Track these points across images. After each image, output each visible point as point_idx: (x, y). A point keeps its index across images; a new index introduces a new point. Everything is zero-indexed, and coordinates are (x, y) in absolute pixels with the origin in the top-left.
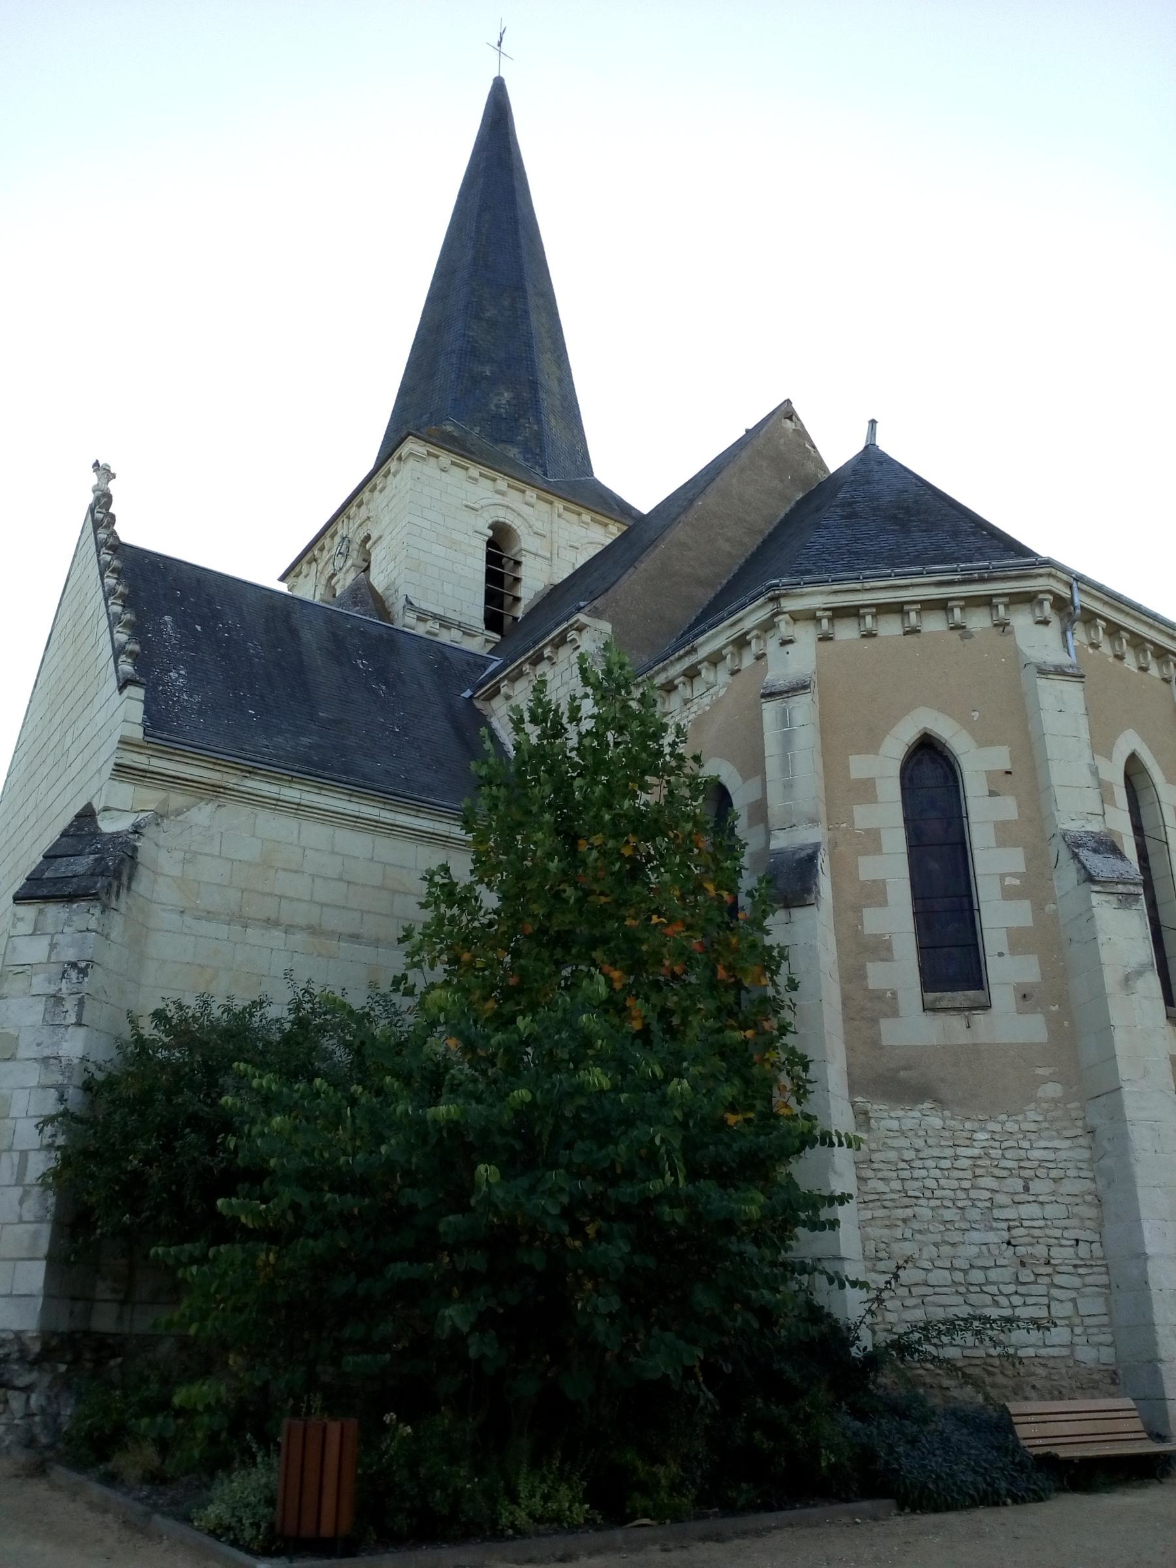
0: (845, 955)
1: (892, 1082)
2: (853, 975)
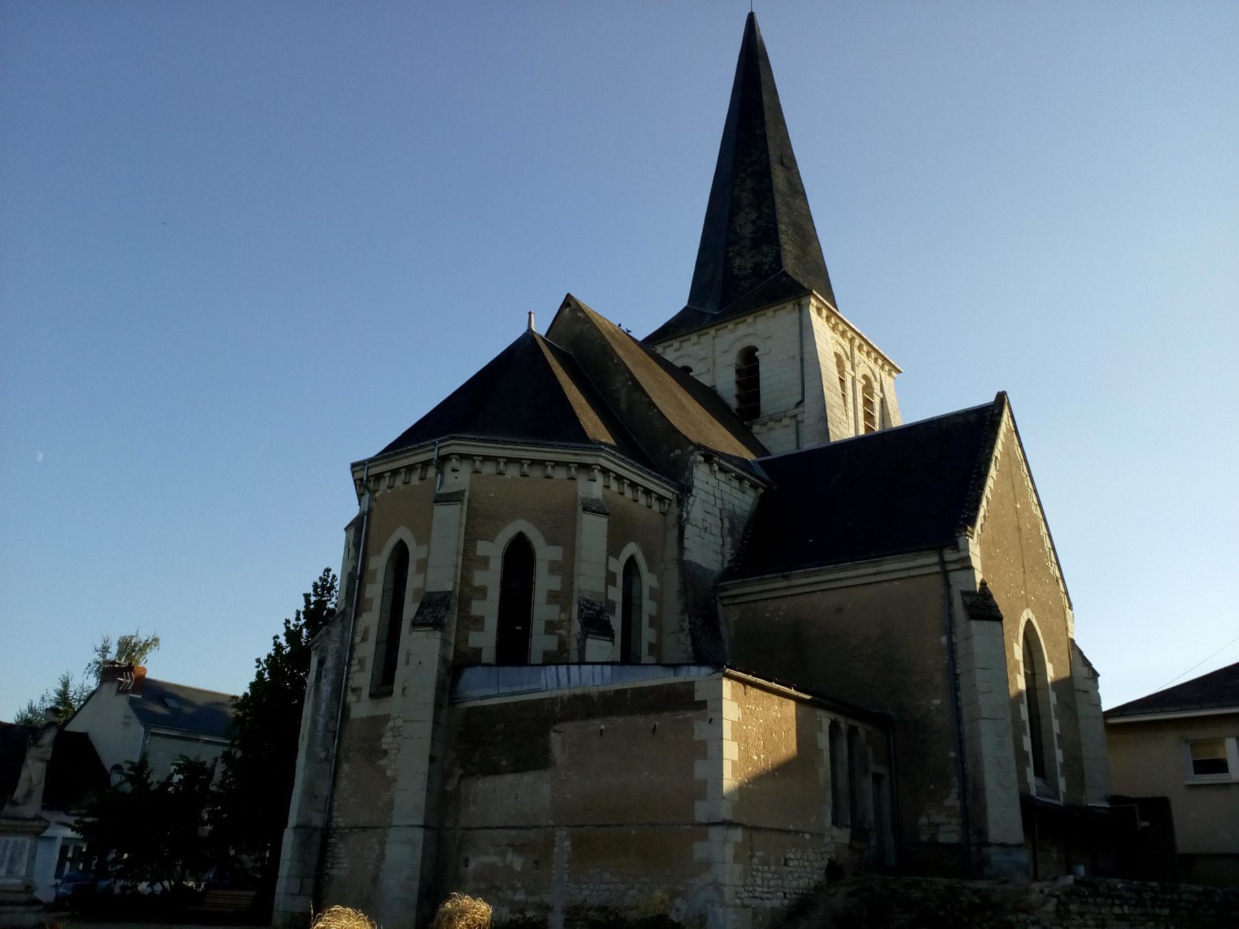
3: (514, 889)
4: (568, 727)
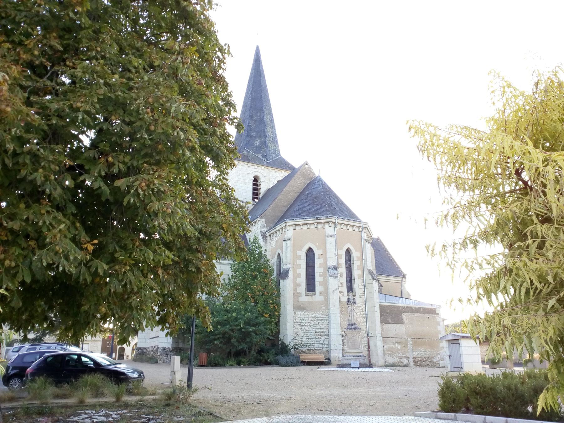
0: (291, 289)
1: (299, 307)
2: (295, 290)
3: (399, 353)
4: (408, 314)
